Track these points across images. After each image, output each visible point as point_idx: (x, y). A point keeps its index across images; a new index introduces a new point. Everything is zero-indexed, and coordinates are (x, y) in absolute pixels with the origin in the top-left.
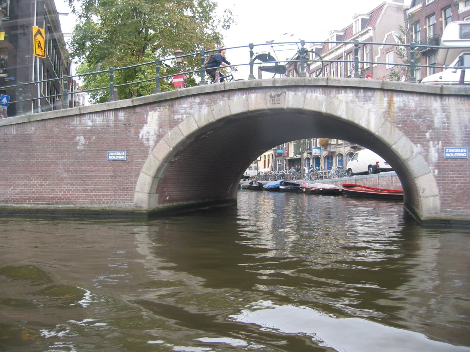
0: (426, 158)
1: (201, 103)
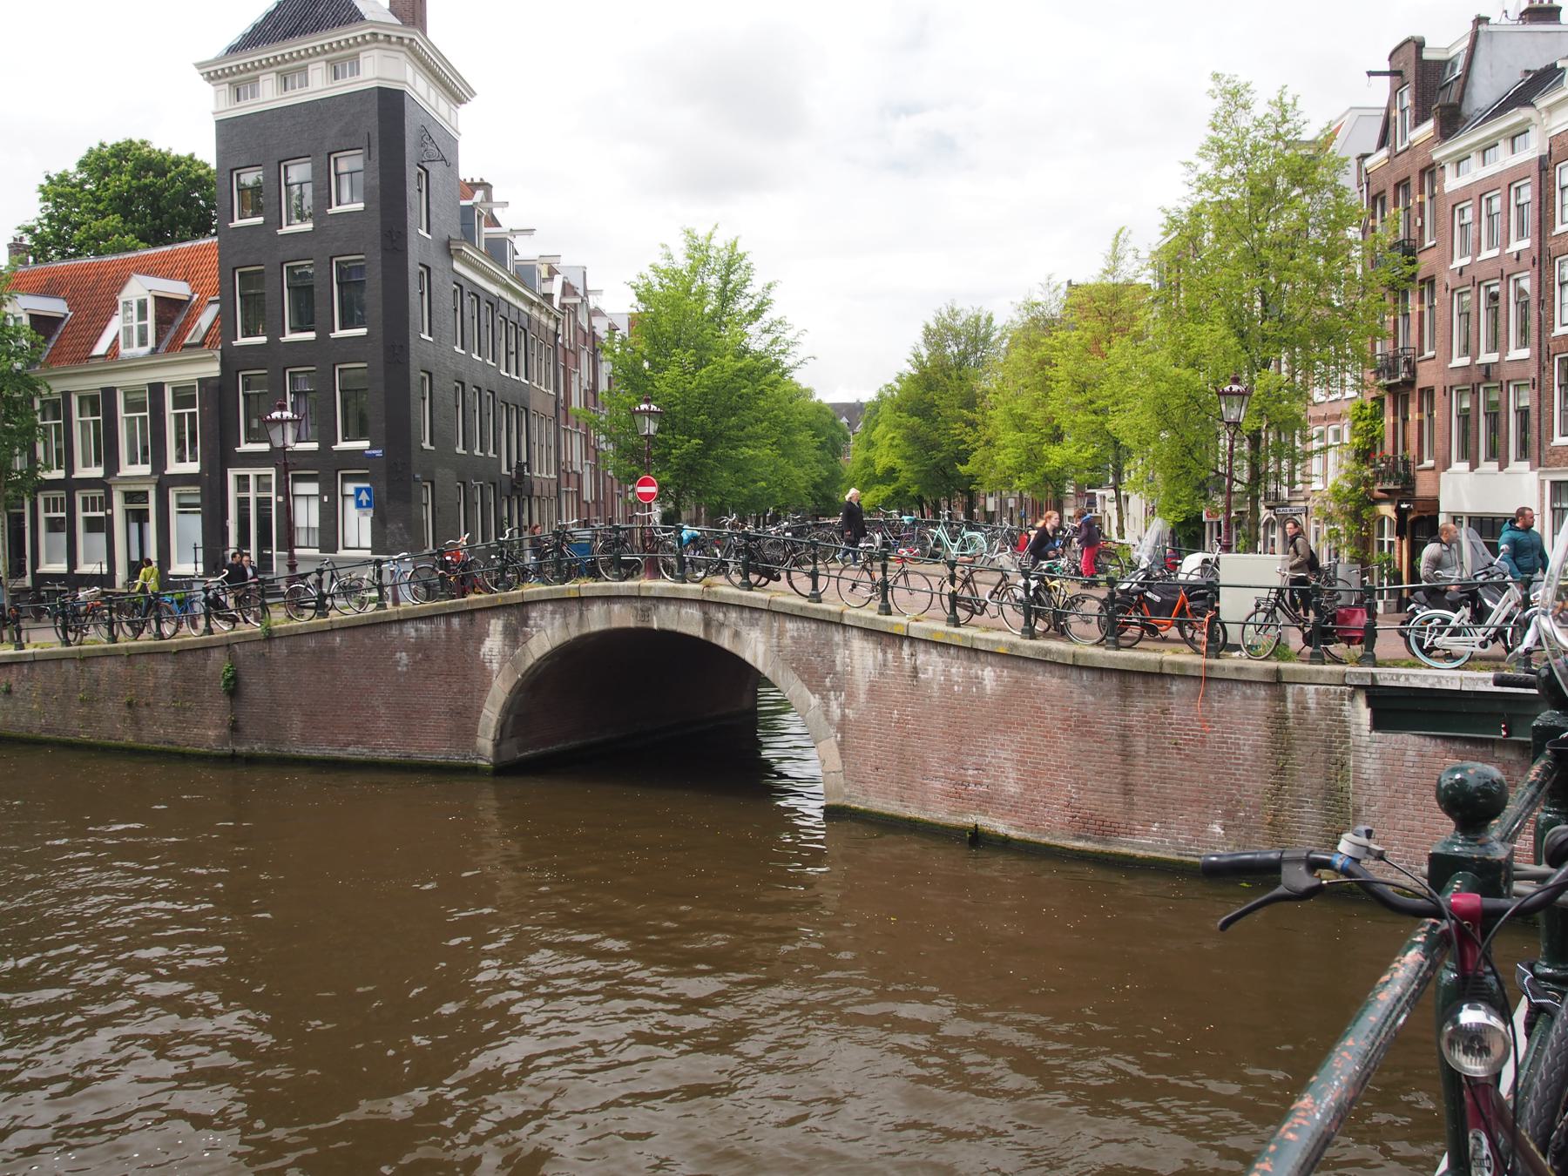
1: (553, 613)
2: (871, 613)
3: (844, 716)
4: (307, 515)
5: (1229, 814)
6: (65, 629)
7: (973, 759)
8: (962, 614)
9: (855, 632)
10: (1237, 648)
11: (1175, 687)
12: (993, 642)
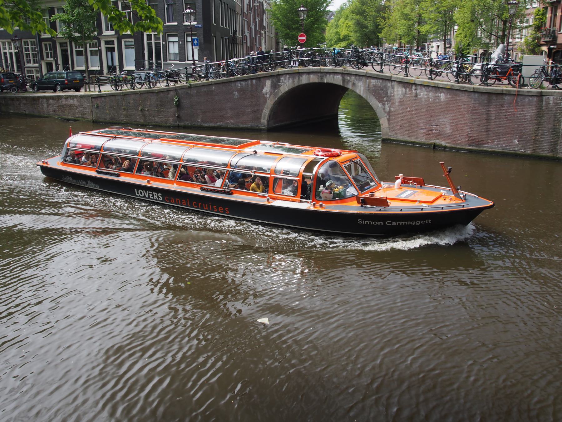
0: (384, 109)
1: (289, 78)
2: (401, 76)
3: (390, 110)
4: (174, 48)
5: (521, 137)
6: (116, 86)
7: (435, 122)
8: (433, 76)
9: (395, 83)
10: (527, 85)
11: (506, 98)
12: (445, 85)
